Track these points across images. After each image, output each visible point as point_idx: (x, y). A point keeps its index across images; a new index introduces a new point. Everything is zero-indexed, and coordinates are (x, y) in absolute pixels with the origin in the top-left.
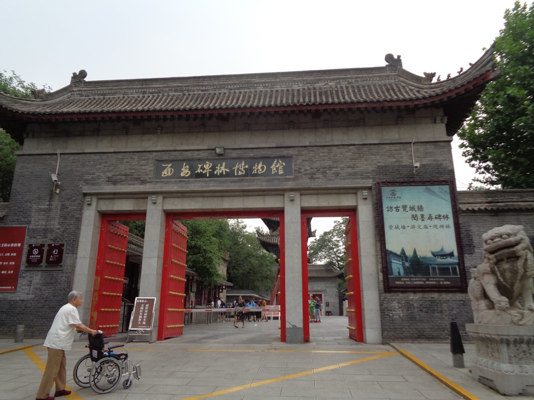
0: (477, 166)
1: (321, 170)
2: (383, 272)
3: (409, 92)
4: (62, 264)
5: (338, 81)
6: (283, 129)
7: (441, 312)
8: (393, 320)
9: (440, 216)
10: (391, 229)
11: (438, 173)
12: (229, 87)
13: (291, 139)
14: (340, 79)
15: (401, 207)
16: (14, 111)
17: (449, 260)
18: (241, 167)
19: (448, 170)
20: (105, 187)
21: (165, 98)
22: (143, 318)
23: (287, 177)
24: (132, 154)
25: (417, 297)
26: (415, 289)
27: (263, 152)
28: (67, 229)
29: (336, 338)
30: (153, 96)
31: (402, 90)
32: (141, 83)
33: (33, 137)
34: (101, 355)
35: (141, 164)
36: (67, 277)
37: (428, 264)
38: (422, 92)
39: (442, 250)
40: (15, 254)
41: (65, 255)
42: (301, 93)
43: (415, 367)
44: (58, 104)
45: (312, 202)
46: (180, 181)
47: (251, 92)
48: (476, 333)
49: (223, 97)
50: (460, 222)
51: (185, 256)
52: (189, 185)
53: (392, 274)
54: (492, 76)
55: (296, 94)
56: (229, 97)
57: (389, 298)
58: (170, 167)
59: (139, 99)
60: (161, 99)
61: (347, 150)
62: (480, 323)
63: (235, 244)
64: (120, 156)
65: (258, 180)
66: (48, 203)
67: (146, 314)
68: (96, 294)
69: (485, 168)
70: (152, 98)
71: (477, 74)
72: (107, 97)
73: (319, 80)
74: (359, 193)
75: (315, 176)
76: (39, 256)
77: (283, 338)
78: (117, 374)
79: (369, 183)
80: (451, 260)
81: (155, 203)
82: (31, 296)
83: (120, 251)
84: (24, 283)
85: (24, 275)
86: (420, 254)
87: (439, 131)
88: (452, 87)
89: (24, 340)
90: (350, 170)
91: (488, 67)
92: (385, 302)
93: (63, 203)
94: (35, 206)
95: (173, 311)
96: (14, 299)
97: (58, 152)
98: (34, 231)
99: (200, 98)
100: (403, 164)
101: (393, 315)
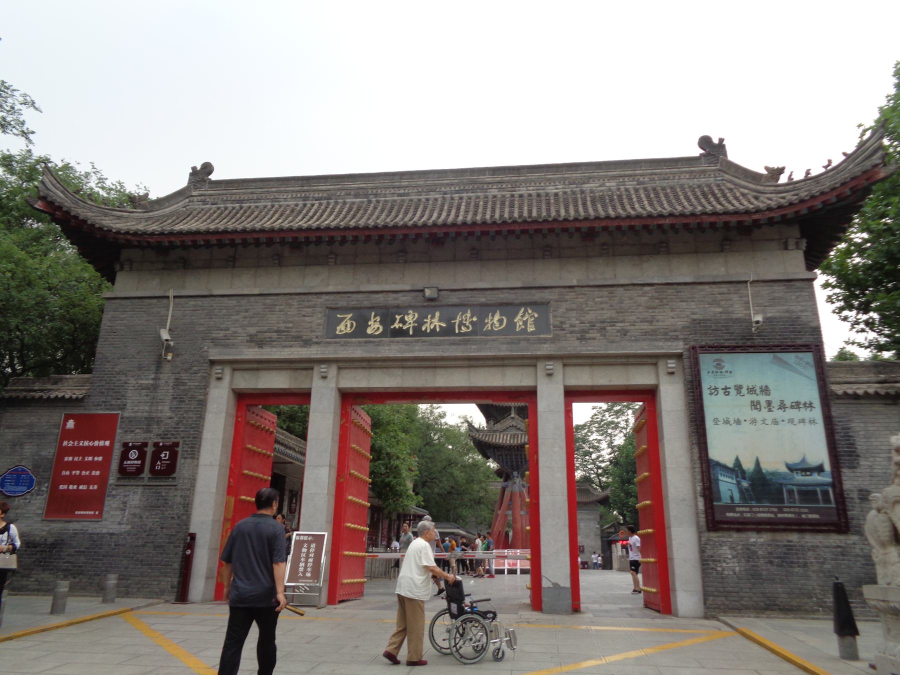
0: (852, 319)
1: (598, 325)
2: (704, 496)
3: (741, 198)
4: (174, 475)
5: (621, 180)
6: (532, 257)
7: (805, 565)
8: (722, 578)
9: (798, 403)
10: (716, 424)
11: (791, 332)
12: (443, 189)
13: (548, 274)
14: (625, 176)
15: (733, 388)
16: (105, 229)
17: (816, 478)
18: (465, 319)
19: (811, 328)
20: (245, 350)
21: (339, 207)
22: (306, 567)
23: (542, 336)
24: (288, 297)
25: (762, 540)
26: (759, 526)
27: (502, 296)
28: (184, 418)
29: (622, 606)
30: (320, 204)
31: (729, 195)
32: (300, 182)
33: (131, 270)
34: (461, 611)
35: (304, 313)
36: (184, 497)
37: (781, 484)
38: (763, 198)
39: (804, 460)
40: (100, 458)
41: (180, 461)
42: (561, 200)
43: (773, 656)
44: (168, 216)
45: (583, 378)
46: (365, 342)
47: (478, 197)
48: (883, 601)
49: (434, 205)
50: (834, 414)
51: (367, 465)
52: (380, 348)
53: (719, 499)
54: (882, 175)
55: (552, 201)
56: (443, 205)
57: (716, 539)
58: (351, 319)
59: (298, 208)
60: (333, 209)
61: (640, 292)
62: (889, 584)
63: (427, 444)
64: (269, 301)
65: (493, 340)
66: (153, 376)
67: (311, 560)
68: (228, 525)
69: (867, 323)
70: (319, 208)
71: (858, 170)
72: (245, 205)
73: (590, 178)
74: (661, 364)
75: (588, 336)
76: (139, 462)
77: (537, 604)
78: (484, 640)
79: (678, 347)
80: (820, 478)
81: (324, 378)
82: (125, 528)
83: (264, 455)
84: (114, 506)
85: (114, 492)
86: (767, 466)
87: (792, 263)
88: (815, 190)
89: (117, 600)
90: (646, 326)
91: (876, 159)
92: (709, 547)
93: (178, 376)
94: (132, 381)
95: (351, 556)
96: (98, 531)
97: (171, 293)
98: (131, 421)
99: (396, 207)
100: (734, 316)
101: (724, 569)
